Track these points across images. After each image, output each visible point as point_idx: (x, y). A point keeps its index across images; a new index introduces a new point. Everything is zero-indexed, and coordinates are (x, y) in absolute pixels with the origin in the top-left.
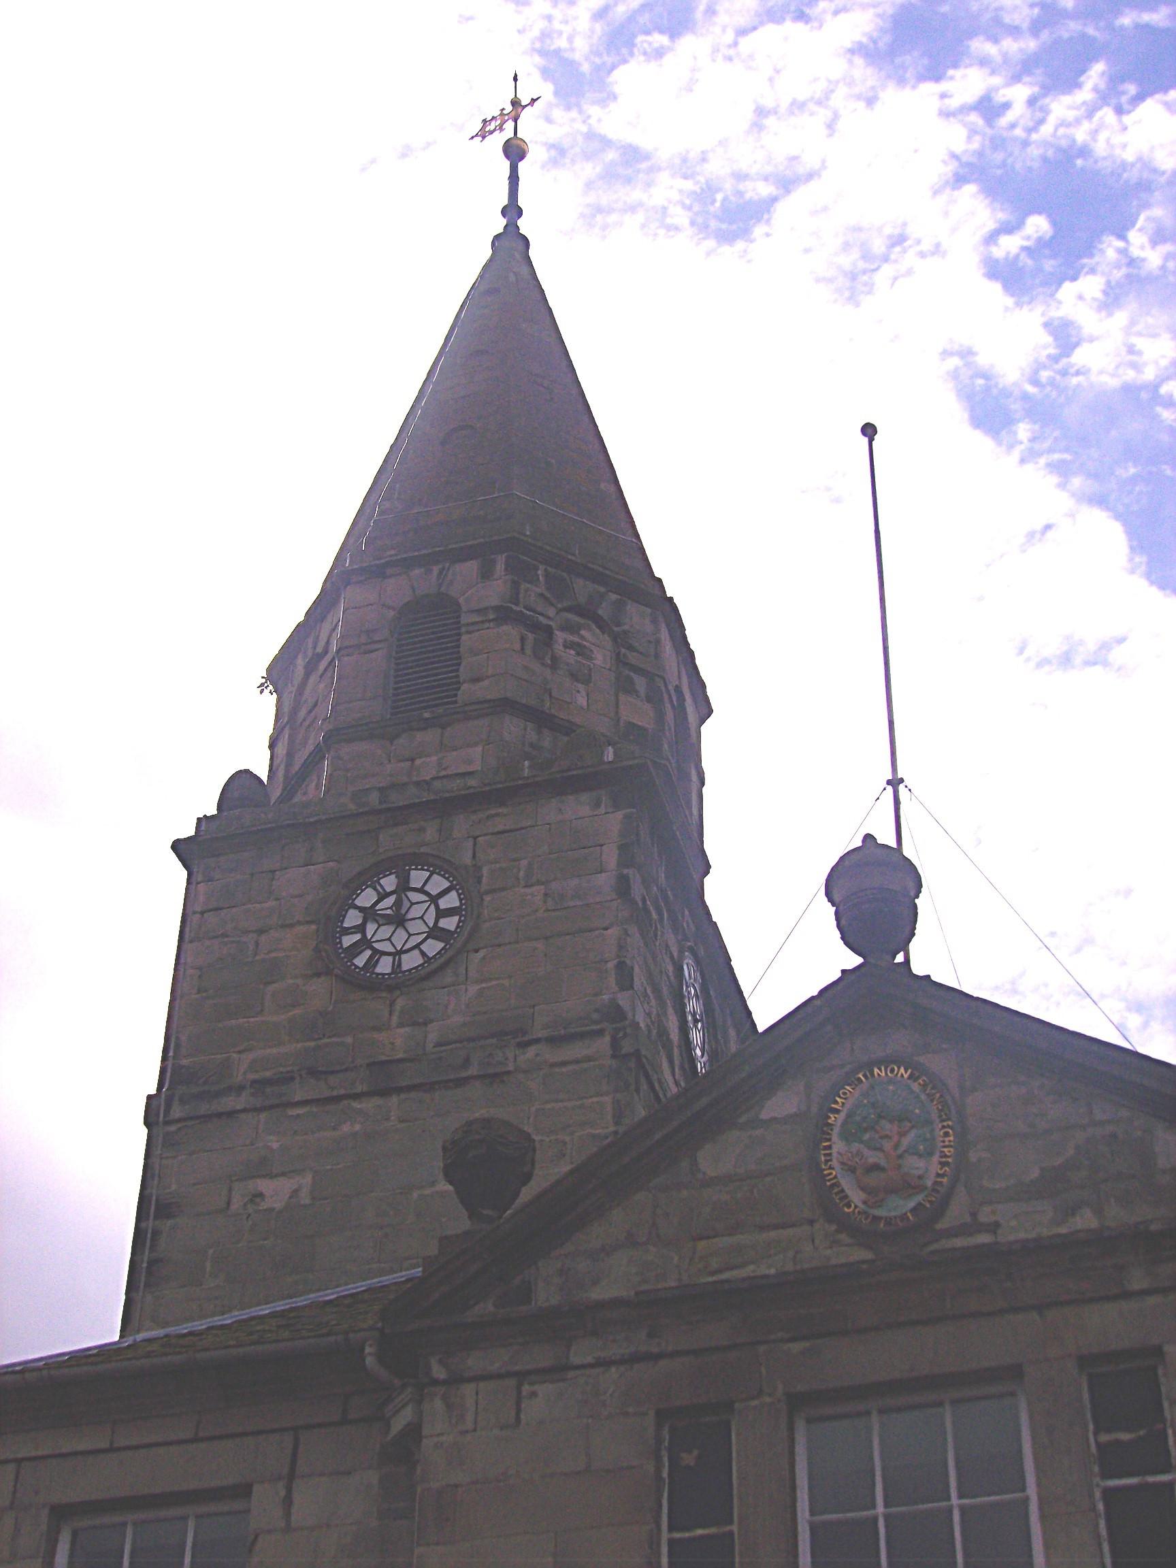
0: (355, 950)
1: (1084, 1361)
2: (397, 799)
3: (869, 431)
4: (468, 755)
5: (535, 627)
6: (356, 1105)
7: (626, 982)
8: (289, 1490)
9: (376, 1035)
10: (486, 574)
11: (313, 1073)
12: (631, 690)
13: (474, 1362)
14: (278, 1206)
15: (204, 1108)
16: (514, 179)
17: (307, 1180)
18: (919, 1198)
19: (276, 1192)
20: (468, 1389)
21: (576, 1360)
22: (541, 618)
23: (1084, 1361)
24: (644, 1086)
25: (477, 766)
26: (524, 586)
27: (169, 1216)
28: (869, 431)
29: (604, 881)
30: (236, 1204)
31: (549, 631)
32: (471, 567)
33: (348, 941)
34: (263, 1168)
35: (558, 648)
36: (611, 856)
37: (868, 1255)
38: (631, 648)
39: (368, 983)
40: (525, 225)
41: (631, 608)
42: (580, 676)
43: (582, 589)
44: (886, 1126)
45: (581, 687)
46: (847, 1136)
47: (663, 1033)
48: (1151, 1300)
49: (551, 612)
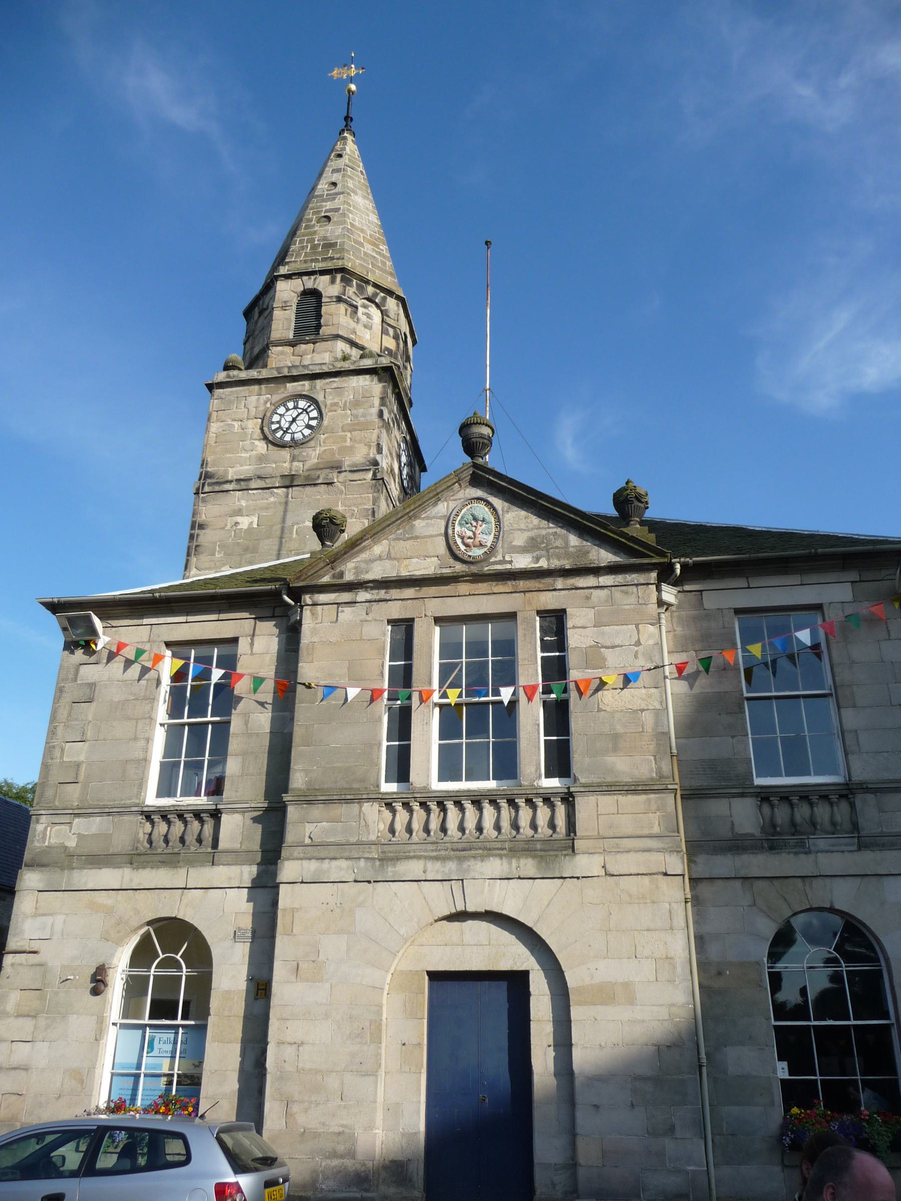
0: (276, 431)
2: (295, 373)
5: (352, 305)
7: (379, 450)
8: (252, 640)
10: (333, 281)
11: (259, 477)
12: (388, 334)
15: (217, 488)
17: (255, 520)
18: (485, 550)
19: (244, 522)
21: (358, 599)
22: (405, 472)
24: (385, 490)
25: (327, 361)
26: (348, 288)
27: (203, 529)
29: (375, 411)
30: (228, 527)
31: (356, 307)
32: (327, 278)
33: (274, 427)
34: (239, 512)
36: (377, 402)
38: (388, 316)
41: (389, 299)
42: (368, 327)
45: (368, 331)
46: (460, 524)
47: (392, 470)
49: (358, 299)
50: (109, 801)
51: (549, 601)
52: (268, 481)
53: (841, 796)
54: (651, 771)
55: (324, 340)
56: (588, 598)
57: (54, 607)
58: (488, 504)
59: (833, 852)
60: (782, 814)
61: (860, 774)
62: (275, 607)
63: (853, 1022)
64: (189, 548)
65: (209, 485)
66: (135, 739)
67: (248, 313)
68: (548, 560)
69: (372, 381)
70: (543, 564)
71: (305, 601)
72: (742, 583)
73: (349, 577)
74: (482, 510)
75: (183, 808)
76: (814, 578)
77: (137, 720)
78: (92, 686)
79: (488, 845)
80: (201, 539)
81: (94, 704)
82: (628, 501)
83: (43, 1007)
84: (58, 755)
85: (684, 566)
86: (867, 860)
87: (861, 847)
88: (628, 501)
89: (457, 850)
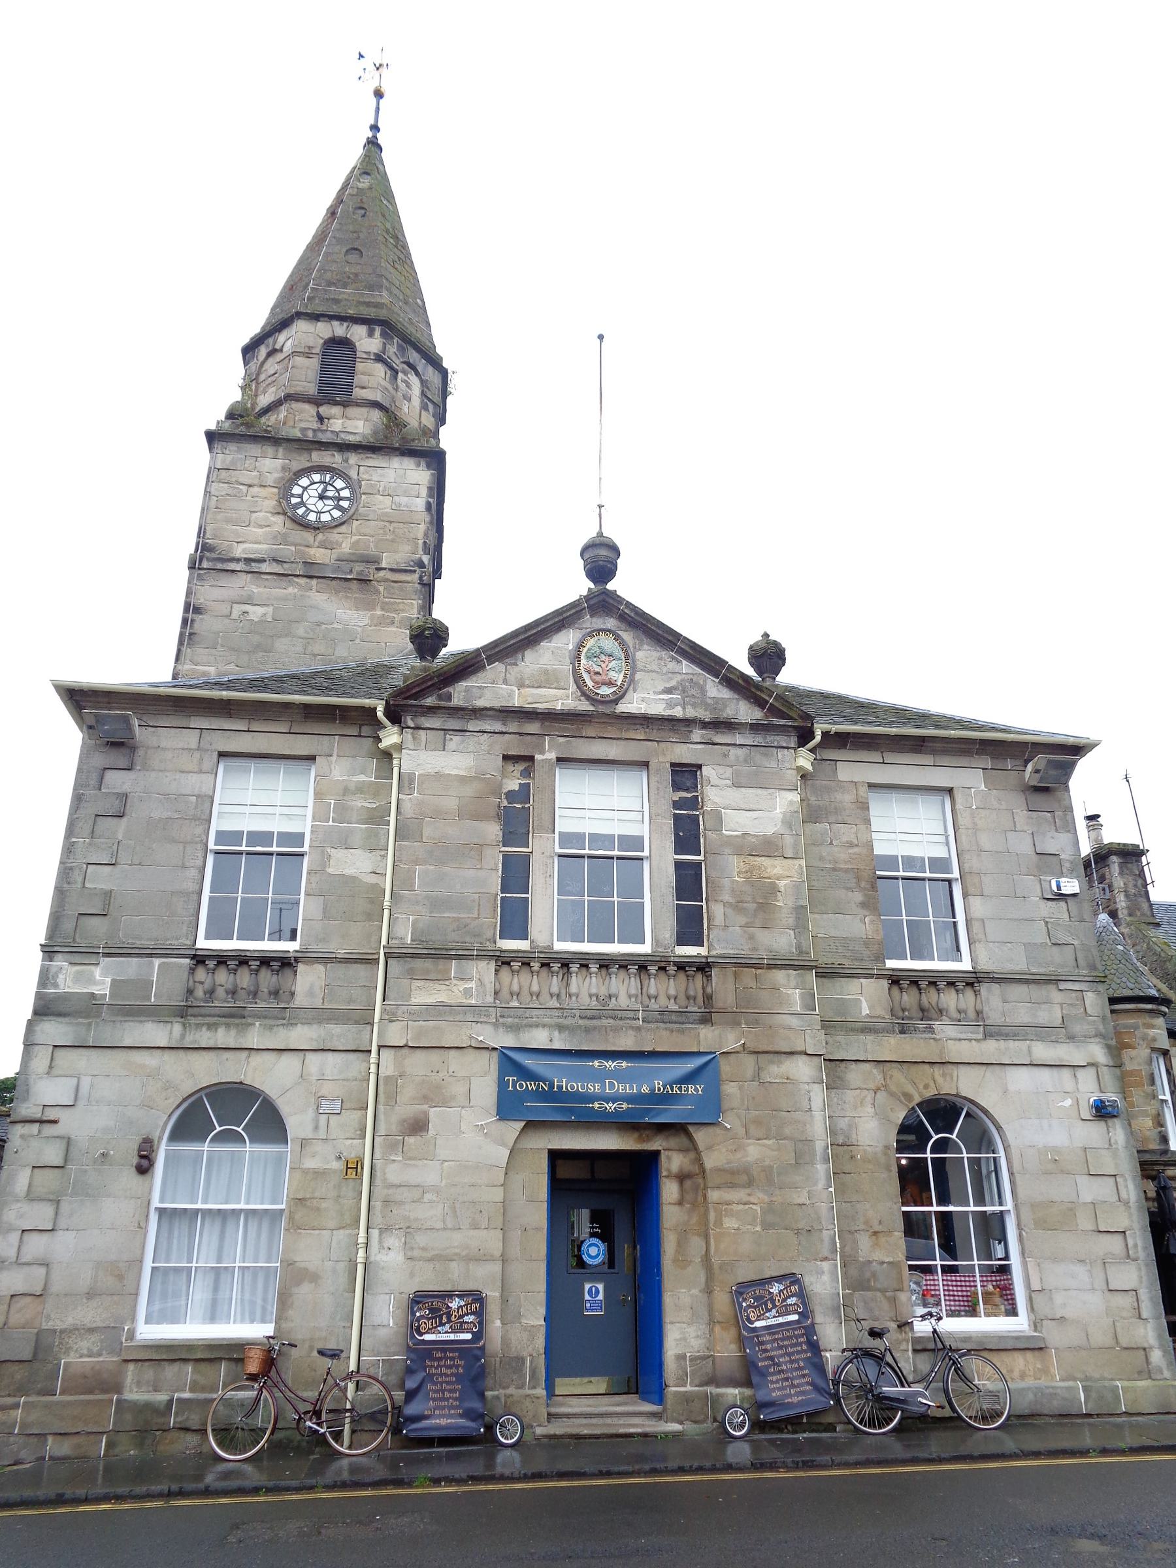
0: (297, 506)
1: (673, 765)
3: (601, 337)
4: (357, 425)
5: (391, 368)
6: (296, 579)
9: (307, 549)
10: (371, 334)
12: (427, 409)
13: (427, 722)
14: (256, 619)
15: (219, 566)
16: (378, 109)
17: (271, 609)
19: (255, 613)
20: (422, 732)
23: (673, 765)
27: (200, 613)
28: (601, 337)
33: (294, 500)
34: (249, 601)
35: (399, 380)
37: (592, 708)
39: (304, 525)
40: (382, 139)
43: (414, 356)
44: (603, 657)
46: (588, 658)
48: (700, 746)
50: (148, 940)
51: (684, 753)
52: (285, 565)
53: (968, 984)
54: (791, 946)
55: (358, 405)
56: (725, 755)
57: (77, 698)
58: (617, 638)
59: (960, 1040)
60: (909, 998)
61: (985, 965)
62: (361, 726)
63: (972, 1208)
64: (182, 635)
65: (208, 559)
66: (184, 867)
67: (249, 351)
68: (684, 709)
69: (419, 465)
70: (678, 712)
71: (405, 722)
72: (876, 756)
73: (456, 702)
74: (608, 643)
75: (248, 954)
76: (946, 760)
77: (185, 843)
78: (124, 797)
79: (619, 1014)
80: (196, 625)
81: (125, 819)
82: (769, 656)
83: (68, 1181)
84: (80, 879)
85: (825, 734)
86: (991, 1049)
87: (987, 1035)
88: (769, 656)
89: (585, 1018)
